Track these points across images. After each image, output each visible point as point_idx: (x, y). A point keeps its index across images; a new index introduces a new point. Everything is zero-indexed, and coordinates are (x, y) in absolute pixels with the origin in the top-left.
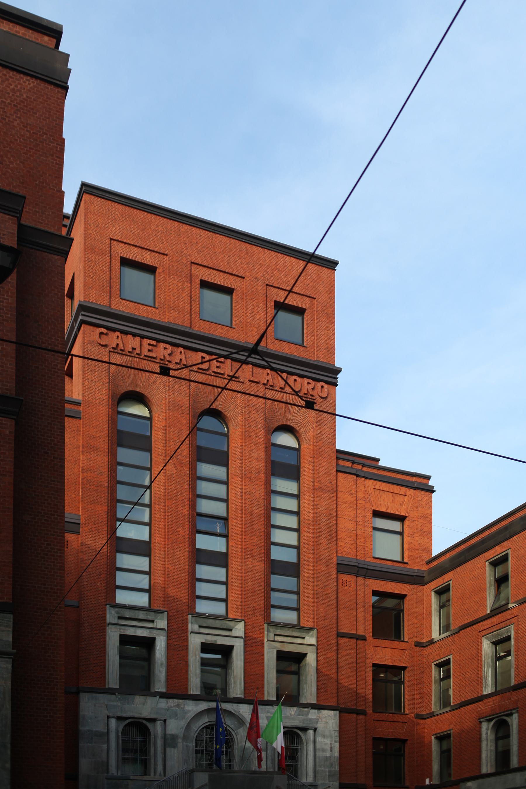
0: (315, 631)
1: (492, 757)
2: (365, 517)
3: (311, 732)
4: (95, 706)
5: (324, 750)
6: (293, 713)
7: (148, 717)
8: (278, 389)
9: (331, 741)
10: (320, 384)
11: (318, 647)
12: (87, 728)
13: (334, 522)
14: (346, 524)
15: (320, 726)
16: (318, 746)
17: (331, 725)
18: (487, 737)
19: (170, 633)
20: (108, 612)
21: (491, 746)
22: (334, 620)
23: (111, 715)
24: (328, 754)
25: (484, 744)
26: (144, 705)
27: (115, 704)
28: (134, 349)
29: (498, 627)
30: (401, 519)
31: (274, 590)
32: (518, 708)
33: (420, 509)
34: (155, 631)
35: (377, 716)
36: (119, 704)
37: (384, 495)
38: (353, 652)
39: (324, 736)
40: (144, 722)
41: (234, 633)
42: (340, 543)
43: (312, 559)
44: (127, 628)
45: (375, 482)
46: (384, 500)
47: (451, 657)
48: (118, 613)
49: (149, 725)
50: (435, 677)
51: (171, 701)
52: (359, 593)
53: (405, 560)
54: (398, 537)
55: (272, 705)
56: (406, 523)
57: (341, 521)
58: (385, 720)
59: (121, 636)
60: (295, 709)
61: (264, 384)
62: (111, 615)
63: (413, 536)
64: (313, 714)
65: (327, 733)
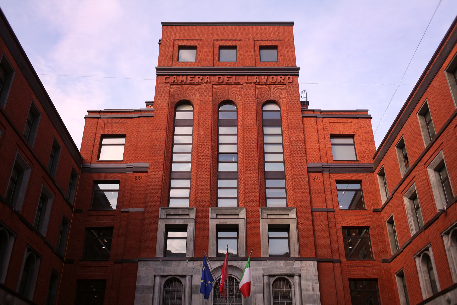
0: (295, 209)
1: (428, 286)
2: (325, 138)
3: (296, 278)
4: (147, 269)
5: (307, 290)
6: (282, 265)
7: (181, 274)
8: (263, 84)
9: (313, 283)
10: (287, 77)
11: (297, 220)
12: (141, 284)
13: (303, 144)
14: (312, 144)
15: (303, 273)
16: (303, 287)
17: (312, 271)
18: (420, 269)
19: (196, 221)
20: (160, 212)
21: (425, 276)
22: (309, 201)
23: (157, 274)
24: (311, 292)
25: (420, 275)
26: (178, 266)
27: (160, 267)
28: (182, 81)
29: (408, 186)
30: (352, 136)
31: (269, 188)
32: (430, 243)
33: (363, 129)
34: (187, 220)
35: (349, 263)
36: (162, 267)
37: (337, 125)
38: (325, 220)
39: (307, 280)
40: (178, 277)
41: (240, 216)
42: (308, 156)
43: (290, 167)
44: (170, 220)
45: (329, 119)
46: (337, 128)
47: (393, 214)
48: (166, 212)
49: (181, 279)
50: (389, 231)
51: (196, 262)
52: (325, 183)
53: (358, 159)
54: (353, 147)
55: (266, 260)
56: (355, 138)
57: (308, 143)
58: (357, 265)
59: (166, 225)
60: (283, 261)
61: (254, 83)
62: (162, 214)
63: (360, 144)
64: (297, 264)
65: (309, 277)
